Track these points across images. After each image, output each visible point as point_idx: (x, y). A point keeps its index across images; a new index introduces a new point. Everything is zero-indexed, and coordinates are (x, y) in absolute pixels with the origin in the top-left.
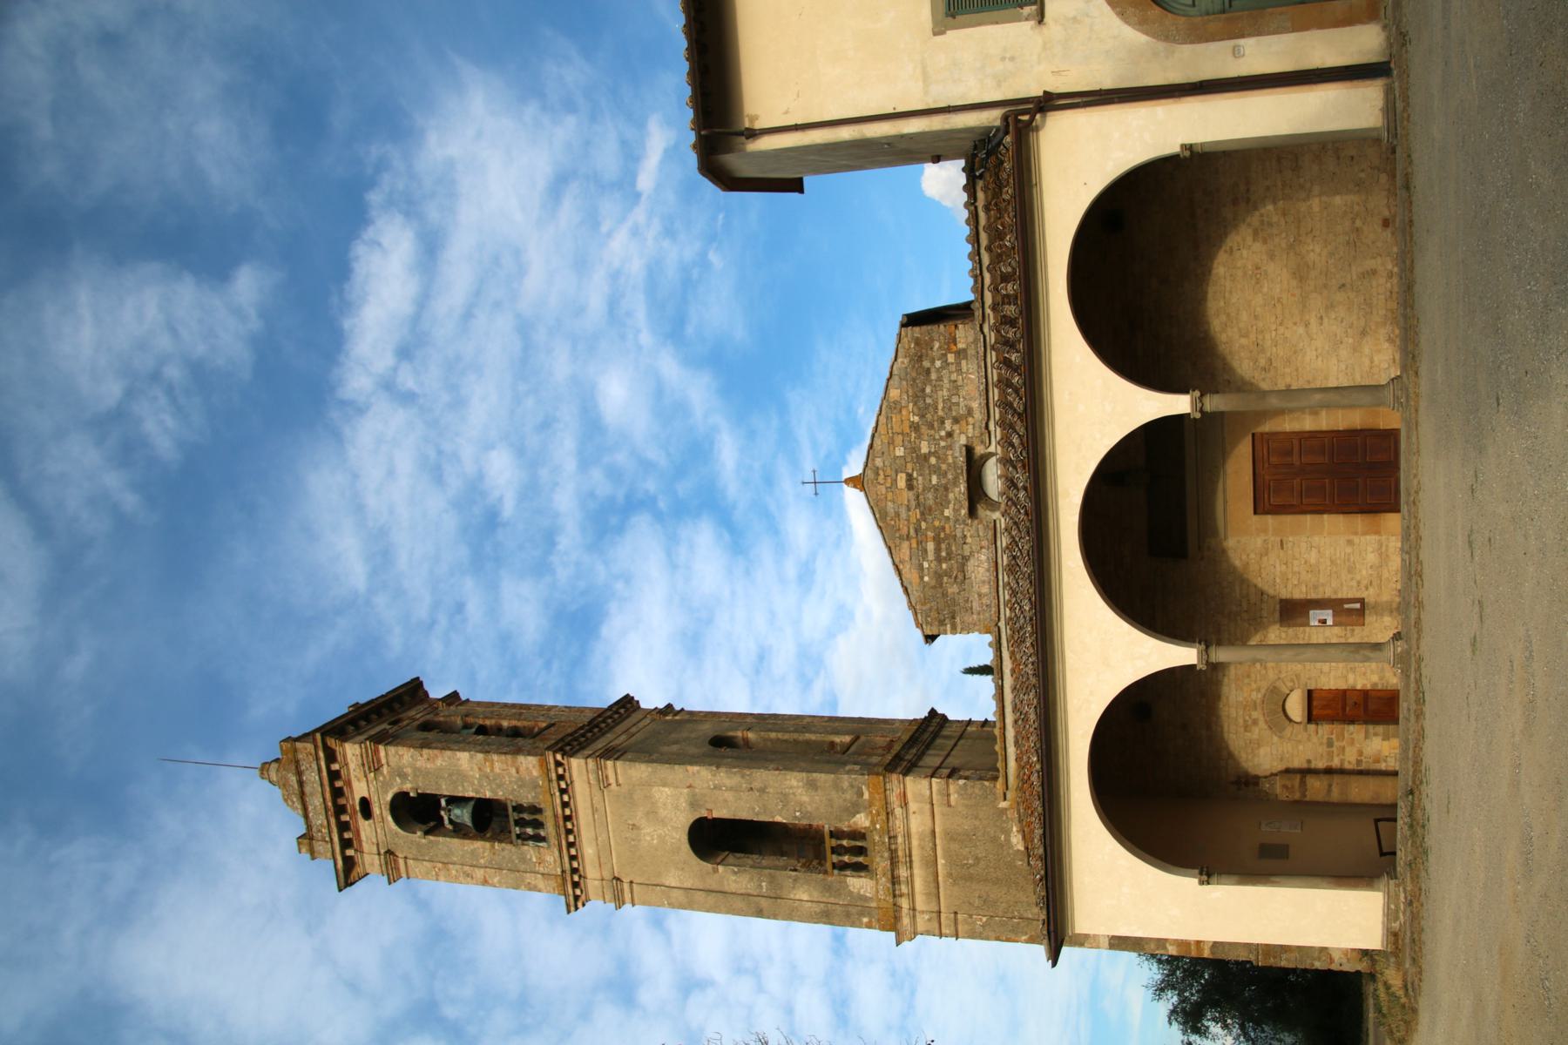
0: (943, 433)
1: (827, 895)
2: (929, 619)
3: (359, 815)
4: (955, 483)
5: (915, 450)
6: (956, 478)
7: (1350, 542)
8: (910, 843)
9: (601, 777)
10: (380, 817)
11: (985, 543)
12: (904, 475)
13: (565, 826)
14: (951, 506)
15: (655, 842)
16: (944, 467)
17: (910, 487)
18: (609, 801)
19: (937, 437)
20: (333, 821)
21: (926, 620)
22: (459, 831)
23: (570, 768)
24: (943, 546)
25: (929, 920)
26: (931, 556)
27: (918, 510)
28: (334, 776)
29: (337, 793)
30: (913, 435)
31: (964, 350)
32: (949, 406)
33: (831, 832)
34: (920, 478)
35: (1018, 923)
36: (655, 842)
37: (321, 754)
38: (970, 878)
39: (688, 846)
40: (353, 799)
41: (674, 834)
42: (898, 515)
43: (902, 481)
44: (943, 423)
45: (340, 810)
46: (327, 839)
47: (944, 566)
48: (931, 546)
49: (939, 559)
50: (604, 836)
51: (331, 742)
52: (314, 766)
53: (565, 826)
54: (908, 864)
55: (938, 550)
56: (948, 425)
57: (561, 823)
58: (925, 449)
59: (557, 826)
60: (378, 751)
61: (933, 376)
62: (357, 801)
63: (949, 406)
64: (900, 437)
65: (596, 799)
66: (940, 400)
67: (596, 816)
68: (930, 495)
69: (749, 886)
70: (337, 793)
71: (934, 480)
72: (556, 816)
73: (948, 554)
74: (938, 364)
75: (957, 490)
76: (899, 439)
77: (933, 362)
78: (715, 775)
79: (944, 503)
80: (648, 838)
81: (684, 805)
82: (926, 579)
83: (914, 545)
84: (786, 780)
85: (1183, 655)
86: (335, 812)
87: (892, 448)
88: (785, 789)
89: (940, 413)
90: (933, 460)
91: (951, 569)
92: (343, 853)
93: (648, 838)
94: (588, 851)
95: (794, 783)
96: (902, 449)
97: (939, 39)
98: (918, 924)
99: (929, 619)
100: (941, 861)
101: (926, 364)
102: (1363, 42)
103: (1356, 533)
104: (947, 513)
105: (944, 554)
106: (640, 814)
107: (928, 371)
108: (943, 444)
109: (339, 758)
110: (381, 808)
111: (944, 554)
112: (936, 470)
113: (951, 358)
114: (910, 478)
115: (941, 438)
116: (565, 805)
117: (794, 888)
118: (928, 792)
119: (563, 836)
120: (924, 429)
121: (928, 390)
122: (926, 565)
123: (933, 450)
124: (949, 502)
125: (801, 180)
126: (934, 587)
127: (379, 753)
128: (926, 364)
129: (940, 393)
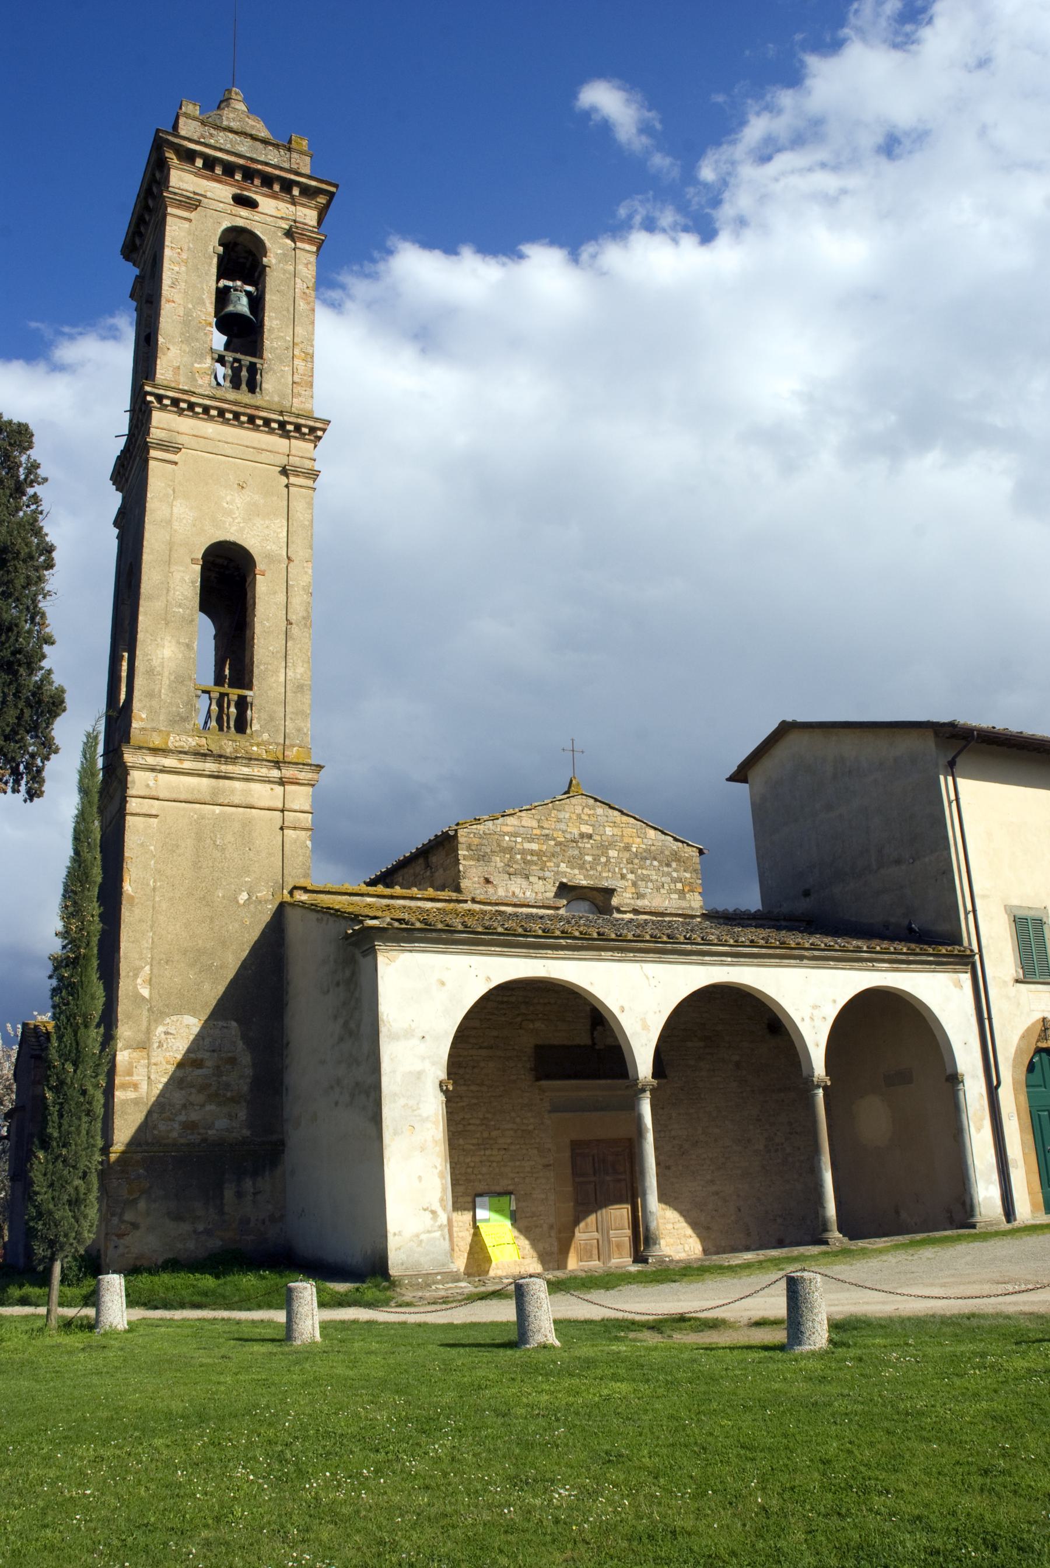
0: (625, 871)
1: (172, 678)
2: (472, 835)
3: (239, 192)
4: (586, 877)
5: (611, 845)
6: (590, 877)
7: (551, 1227)
8: (238, 779)
9: (299, 470)
10: (237, 213)
11: (540, 897)
12: (590, 831)
13: (244, 414)
14: (568, 870)
15: (225, 504)
16: (599, 868)
17: (582, 836)
18: (268, 470)
19: (622, 866)
20: (241, 162)
21: (471, 833)
22: (222, 296)
23: (305, 440)
24: (535, 858)
25: (148, 786)
26: (527, 846)
27: (563, 839)
28: (287, 186)
29: (268, 181)
30: (622, 845)
31: (684, 898)
32: (646, 879)
33: (246, 697)
34: (589, 846)
35: (148, 885)
36: (225, 504)
37: (314, 183)
38: (199, 838)
39: (222, 539)
40: (256, 193)
41: (234, 528)
42: (559, 821)
43: (586, 829)
44: (632, 872)
45: (249, 175)
46: (202, 140)
47: (519, 857)
48: (534, 846)
49: (523, 852)
50: (229, 452)
51: (322, 200)
52: (286, 165)
53: (244, 414)
54: (216, 774)
55: (532, 853)
56: (631, 876)
57: (249, 411)
58: (612, 853)
59: (246, 406)
60: (311, 244)
61: (666, 869)
62: (254, 196)
63: (646, 879)
64: (620, 833)
65: (271, 456)
66: (649, 873)
67: (252, 450)
68: (576, 852)
69: (177, 593)
70: (268, 181)
71: (589, 858)
72: (257, 408)
73: (529, 861)
74: (675, 874)
75: (582, 877)
76: (619, 832)
77: (675, 870)
78: (304, 589)
79: (570, 864)
80: (228, 498)
81: (268, 547)
82: (507, 838)
83: (535, 831)
84: (303, 661)
85: (644, 1065)
86: (249, 168)
87: (612, 825)
88: (292, 658)
89: (640, 871)
90: (603, 859)
91: (516, 862)
92: (202, 155)
93: (228, 498)
94: (211, 429)
95: (300, 670)
96: (611, 834)
97: (1003, 909)
98: (142, 773)
99: (472, 835)
100: (218, 809)
101: (674, 865)
102: (1025, 1209)
103: (560, 1232)
104: (563, 865)
105: (529, 858)
106: (256, 497)
107: (668, 865)
108: (617, 869)
109: (304, 200)
110: (243, 218)
111: (529, 858)
112: (596, 858)
113: (679, 886)
114: (590, 837)
115: (621, 869)
116: (267, 422)
117: (179, 643)
118: (297, 807)
119: (234, 408)
120: (627, 855)
121: (656, 863)
122: (519, 840)
123: (612, 860)
124: (572, 869)
125: (745, 780)
126: (499, 845)
127: (309, 244)
128: (674, 865)
129: (654, 873)
